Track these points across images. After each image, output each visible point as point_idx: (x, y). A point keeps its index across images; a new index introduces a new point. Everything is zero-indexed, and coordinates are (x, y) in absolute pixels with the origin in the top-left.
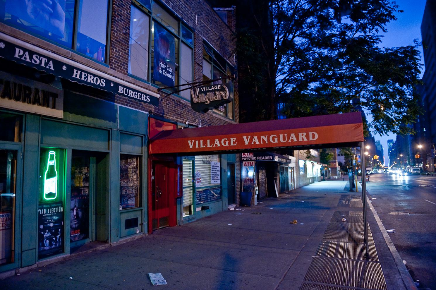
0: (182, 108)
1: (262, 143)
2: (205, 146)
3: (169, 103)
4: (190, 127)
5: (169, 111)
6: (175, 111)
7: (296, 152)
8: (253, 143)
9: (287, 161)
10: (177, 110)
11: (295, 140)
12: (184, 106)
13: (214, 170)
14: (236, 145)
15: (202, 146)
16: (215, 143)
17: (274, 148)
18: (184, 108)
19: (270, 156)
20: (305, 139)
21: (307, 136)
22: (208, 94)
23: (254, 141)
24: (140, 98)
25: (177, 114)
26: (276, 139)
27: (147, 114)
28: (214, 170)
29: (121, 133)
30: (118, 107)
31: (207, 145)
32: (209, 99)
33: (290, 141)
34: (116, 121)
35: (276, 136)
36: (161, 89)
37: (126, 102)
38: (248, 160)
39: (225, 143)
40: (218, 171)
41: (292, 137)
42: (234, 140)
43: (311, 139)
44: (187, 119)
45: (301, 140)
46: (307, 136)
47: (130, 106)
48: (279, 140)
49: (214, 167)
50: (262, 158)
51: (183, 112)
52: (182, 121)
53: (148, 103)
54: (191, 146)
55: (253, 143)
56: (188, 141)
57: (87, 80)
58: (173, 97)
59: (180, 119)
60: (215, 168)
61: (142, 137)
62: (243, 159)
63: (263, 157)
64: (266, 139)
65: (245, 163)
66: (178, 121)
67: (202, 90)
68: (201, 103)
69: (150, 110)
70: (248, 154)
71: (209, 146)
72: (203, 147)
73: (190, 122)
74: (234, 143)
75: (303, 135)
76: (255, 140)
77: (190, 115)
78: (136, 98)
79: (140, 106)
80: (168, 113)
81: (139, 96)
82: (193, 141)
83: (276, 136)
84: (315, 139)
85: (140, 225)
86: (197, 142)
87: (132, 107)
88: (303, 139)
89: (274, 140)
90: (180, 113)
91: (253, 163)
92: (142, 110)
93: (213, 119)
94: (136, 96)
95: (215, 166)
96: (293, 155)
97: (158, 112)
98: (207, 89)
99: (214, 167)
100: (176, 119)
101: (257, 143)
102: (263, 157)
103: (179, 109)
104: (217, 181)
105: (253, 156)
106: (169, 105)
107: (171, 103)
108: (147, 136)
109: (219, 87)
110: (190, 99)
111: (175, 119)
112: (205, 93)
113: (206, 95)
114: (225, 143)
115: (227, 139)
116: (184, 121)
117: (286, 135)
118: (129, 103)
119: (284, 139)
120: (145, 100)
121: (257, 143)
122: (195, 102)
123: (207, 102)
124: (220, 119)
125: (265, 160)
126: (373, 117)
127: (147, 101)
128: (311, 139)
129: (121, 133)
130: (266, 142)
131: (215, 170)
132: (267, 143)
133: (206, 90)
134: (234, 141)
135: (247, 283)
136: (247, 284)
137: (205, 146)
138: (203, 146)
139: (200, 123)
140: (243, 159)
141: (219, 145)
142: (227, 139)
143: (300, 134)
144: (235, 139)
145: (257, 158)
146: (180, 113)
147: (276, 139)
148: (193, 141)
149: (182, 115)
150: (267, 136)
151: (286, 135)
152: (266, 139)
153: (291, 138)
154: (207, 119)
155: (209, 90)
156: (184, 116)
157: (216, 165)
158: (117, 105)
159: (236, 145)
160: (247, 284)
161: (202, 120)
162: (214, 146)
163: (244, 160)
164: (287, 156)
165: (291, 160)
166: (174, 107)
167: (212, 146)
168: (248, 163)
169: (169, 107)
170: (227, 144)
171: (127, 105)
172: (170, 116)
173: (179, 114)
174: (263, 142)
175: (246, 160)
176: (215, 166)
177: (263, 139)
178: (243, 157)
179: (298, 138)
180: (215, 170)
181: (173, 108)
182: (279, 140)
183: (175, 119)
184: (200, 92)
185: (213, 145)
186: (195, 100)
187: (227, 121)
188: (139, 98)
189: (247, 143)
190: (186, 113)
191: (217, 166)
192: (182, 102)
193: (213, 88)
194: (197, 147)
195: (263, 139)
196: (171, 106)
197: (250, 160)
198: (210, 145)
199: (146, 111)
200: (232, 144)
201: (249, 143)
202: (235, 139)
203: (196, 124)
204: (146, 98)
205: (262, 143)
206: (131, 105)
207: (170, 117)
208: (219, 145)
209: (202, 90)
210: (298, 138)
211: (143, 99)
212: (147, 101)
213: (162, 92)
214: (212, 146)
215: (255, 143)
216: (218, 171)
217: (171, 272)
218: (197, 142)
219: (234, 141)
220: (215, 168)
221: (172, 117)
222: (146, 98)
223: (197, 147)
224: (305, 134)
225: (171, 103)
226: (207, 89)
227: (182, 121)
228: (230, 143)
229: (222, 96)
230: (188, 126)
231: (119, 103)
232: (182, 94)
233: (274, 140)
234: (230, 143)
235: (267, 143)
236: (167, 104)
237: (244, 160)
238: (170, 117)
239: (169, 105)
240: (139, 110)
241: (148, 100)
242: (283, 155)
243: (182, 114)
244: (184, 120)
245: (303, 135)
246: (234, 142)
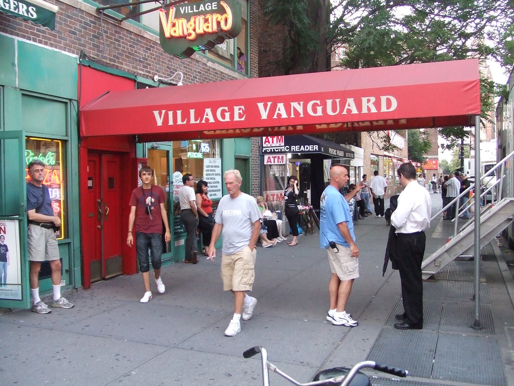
0: (147, 48)
1: (292, 116)
2: (185, 123)
3: (120, 37)
4: (162, 86)
5: (119, 54)
6: (133, 55)
7: (364, 135)
8: (275, 117)
9: (347, 154)
10: (136, 52)
11: (355, 111)
12: (149, 44)
13: (210, 175)
14: (243, 119)
15: (179, 122)
16: (205, 116)
17: (318, 127)
18: (150, 50)
19: (314, 144)
20: (374, 110)
21: (378, 104)
22: (192, 19)
23: (277, 111)
24: (15, 9)
25: (136, 60)
26: (319, 109)
27: (76, 59)
28: (210, 175)
29: (23, 94)
30: (16, 43)
31: (189, 120)
32: (194, 30)
33: (345, 113)
34: (160, 178)
35: (318, 102)
36: (104, 9)
37: (33, 34)
38: (274, 152)
39: (223, 117)
40: (217, 175)
41: (349, 105)
42: (240, 109)
43: (384, 109)
44: (157, 71)
45: (365, 111)
46: (378, 104)
47: (40, 42)
48: (324, 110)
49: (210, 168)
50: (300, 147)
51: (149, 57)
52: (147, 74)
53: (34, 20)
54: (159, 122)
55: (275, 117)
56: (357, 112)
57: (19, 11)
58: (129, 24)
59: (143, 70)
60: (212, 171)
61: (66, 103)
62: (264, 149)
63: (302, 147)
64: (300, 109)
65: (269, 158)
66: (138, 73)
67: (182, 12)
68: (180, 37)
69: (82, 51)
70: (275, 139)
71: (192, 121)
72: (181, 123)
73: (162, 77)
74: (240, 116)
75: (369, 101)
76: (279, 110)
77: (163, 62)
78: (7, 8)
79: (60, 43)
80: (118, 58)
81: (12, 6)
82: (164, 112)
83: (318, 102)
84: (392, 109)
85: (67, 271)
86: (170, 113)
87: (46, 43)
88: (369, 109)
89: (315, 110)
90: (143, 58)
91: (282, 157)
92: (65, 51)
93: (207, 72)
94: (7, 5)
95: (212, 167)
96: (358, 145)
97: (98, 56)
98: (192, 9)
99: (210, 168)
100: (135, 70)
101: (284, 115)
102: (302, 147)
103: (140, 50)
104: (215, 195)
105: (283, 144)
106: (119, 41)
107: (123, 39)
108: (75, 103)
109: (213, 6)
110: (158, 30)
111: (133, 69)
112: (188, 17)
113: (188, 21)
114: (223, 117)
115: (226, 108)
116: (150, 75)
117: (338, 101)
118: (38, 36)
119: (334, 109)
120: (26, 15)
121: (284, 115)
122: (167, 35)
123: (190, 35)
124: (222, 72)
125: (305, 151)
126: (502, 66)
127: (30, 16)
128: (384, 109)
129: (23, 94)
130: (300, 114)
131: (213, 174)
132: (302, 116)
133: (190, 12)
134: (241, 111)
135: (255, 377)
136: (255, 379)
137: (185, 123)
138: (183, 121)
139: (180, 79)
140: (264, 149)
141: (212, 120)
142: (226, 108)
143: (364, 100)
144: (243, 107)
145: (290, 148)
146: (143, 58)
147: (319, 109)
148: (164, 112)
149: (147, 63)
150: (302, 103)
151: (338, 101)
152: (300, 109)
153: (347, 107)
154: (195, 71)
155: (195, 11)
156: (150, 65)
157: (214, 164)
158: (14, 39)
159: (243, 119)
160: (255, 379)
161: (184, 73)
162: (203, 122)
163: (266, 152)
164: (348, 147)
165: (353, 153)
166: (131, 46)
167: (198, 122)
168: (274, 158)
169: (119, 45)
170: (227, 119)
171: (35, 40)
172: (122, 64)
173: (140, 61)
174: (294, 115)
175: (271, 153)
176: (212, 167)
177: (295, 109)
178: (264, 146)
179: (359, 106)
180: (213, 174)
181: (127, 49)
182: (324, 110)
183: (133, 69)
184: (178, 15)
185: (201, 120)
186: (168, 32)
187: (234, 76)
188: (12, 10)
189: (264, 115)
190: (155, 59)
191: (216, 167)
192: (146, 36)
193: (202, 8)
194: (171, 123)
195: (294, 108)
196: (123, 43)
197: (278, 152)
198: (196, 120)
199: (73, 53)
200: (236, 118)
201: (268, 116)
202: (243, 107)
203: (173, 80)
204: (28, 11)
205: (292, 116)
206: (43, 40)
207: (122, 66)
208: (212, 120)
209: (182, 12)
210: (359, 106)
211: (21, 13)
212: (30, 16)
213: (105, 14)
214: (198, 122)
215: (279, 115)
216: (217, 175)
217: (118, 357)
218: (170, 113)
219: (241, 111)
220: (212, 171)
221: (126, 65)
222: (28, 11)
223: (171, 123)
224: (373, 99)
225: (123, 39)
226: (192, 9)
227: (147, 74)
228: (232, 116)
229: (218, 23)
230: (159, 85)
231: (18, 35)
232: (145, 19)
233: (315, 110)
234: (232, 116)
235: (302, 116)
236: (115, 40)
237: (266, 152)
238: (122, 66)
239: (119, 41)
240: (60, 51)
241: (32, 15)
242: (341, 145)
243: (147, 60)
244: (149, 72)
245: (369, 101)
246: (240, 114)
